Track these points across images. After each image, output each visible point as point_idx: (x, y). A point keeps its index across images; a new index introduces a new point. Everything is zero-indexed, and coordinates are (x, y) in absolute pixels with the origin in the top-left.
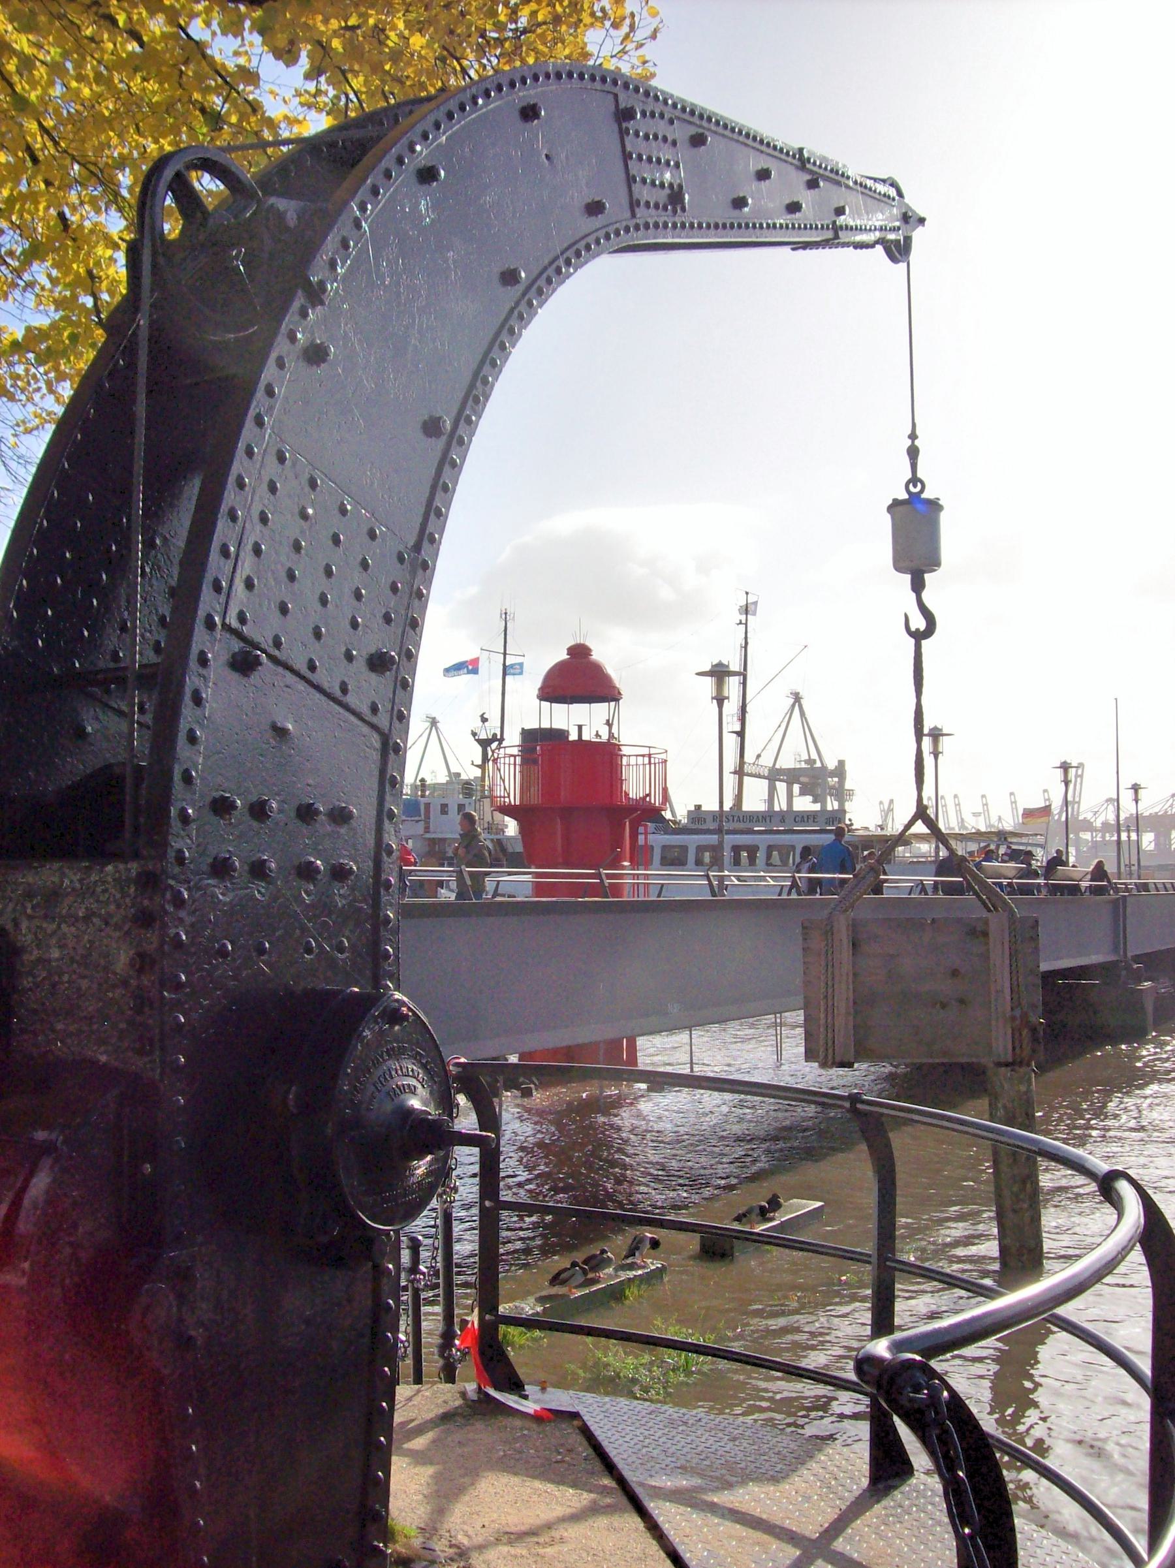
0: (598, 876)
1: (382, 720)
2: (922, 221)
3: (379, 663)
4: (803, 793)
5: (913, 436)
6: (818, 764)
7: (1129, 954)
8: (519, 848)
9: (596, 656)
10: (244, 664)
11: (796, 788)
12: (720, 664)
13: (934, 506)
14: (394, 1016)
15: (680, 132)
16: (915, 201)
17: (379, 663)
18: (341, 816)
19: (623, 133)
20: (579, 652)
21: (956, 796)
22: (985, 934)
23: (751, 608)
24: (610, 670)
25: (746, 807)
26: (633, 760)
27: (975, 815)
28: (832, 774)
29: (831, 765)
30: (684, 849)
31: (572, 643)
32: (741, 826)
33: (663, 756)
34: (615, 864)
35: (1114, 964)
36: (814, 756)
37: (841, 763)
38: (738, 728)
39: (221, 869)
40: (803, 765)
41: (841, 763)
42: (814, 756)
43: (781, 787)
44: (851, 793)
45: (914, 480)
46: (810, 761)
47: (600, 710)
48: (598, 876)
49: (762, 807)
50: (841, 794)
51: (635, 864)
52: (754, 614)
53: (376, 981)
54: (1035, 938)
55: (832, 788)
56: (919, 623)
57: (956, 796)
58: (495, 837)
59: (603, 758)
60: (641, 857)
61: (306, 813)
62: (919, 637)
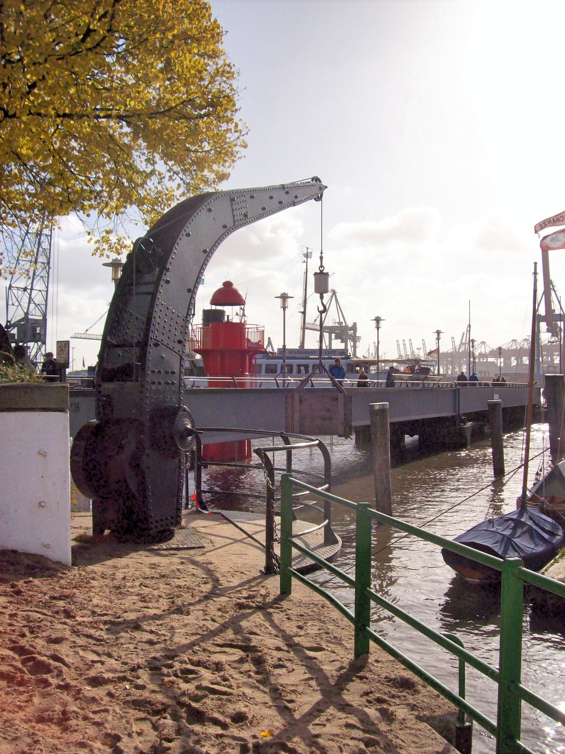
0: (233, 379)
1: (180, 353)
2: (326, 187)
3: (180, 342)
4: (336, 338)
5: (322, 253)
6: (344, 324)
7: (461, 413)
8: (202, 364)
9: (235, 286)
10: (156, 345)
11: (333, 336)
12: (284, 294)
13: (327, 274)
14: (185, 410)
15: (248, 196)
16: (324, 183)
17: (180, 342)
18: (173, 373)
19: (232, 204)
20: (228, 285)
21: (410, 340)
22: (337, 399)
23: (309, 255)
24: (241, 292)
25: (306, 347)
26: (250, 330)
27: (419, 349)
28: (351, 329)
29: (350, 324)
30: (276, 366)
31: (225, 281)
32: (303, 356)
33: (262, 329)
34: (242, 374)
35: (453, 417)
36: (342, 320)
37: (355, 324)
38: (302, 310)
39: (153, 383)
40: (337, 325)
41: (355, 324)
42: (342, 320)
43: (326, 335)
44: (359, 338)
45: (321, 266)
46: (340, 323)
47: (237, 308)
48: (233, 379)
49: (316, 346)
50: (355, 339)
51: (252, 373)
52: (311, 257)
53: (179, 404)
54: (351, 401)
55: (351, 335)
56: (321, 308)
57: (410, 340)
58: (190, 359)
59: (239, 329)
60: (255, 370)
61: (167, 372)
62: (322, 313)
